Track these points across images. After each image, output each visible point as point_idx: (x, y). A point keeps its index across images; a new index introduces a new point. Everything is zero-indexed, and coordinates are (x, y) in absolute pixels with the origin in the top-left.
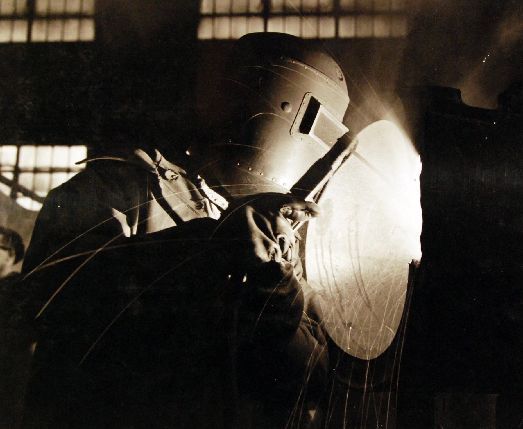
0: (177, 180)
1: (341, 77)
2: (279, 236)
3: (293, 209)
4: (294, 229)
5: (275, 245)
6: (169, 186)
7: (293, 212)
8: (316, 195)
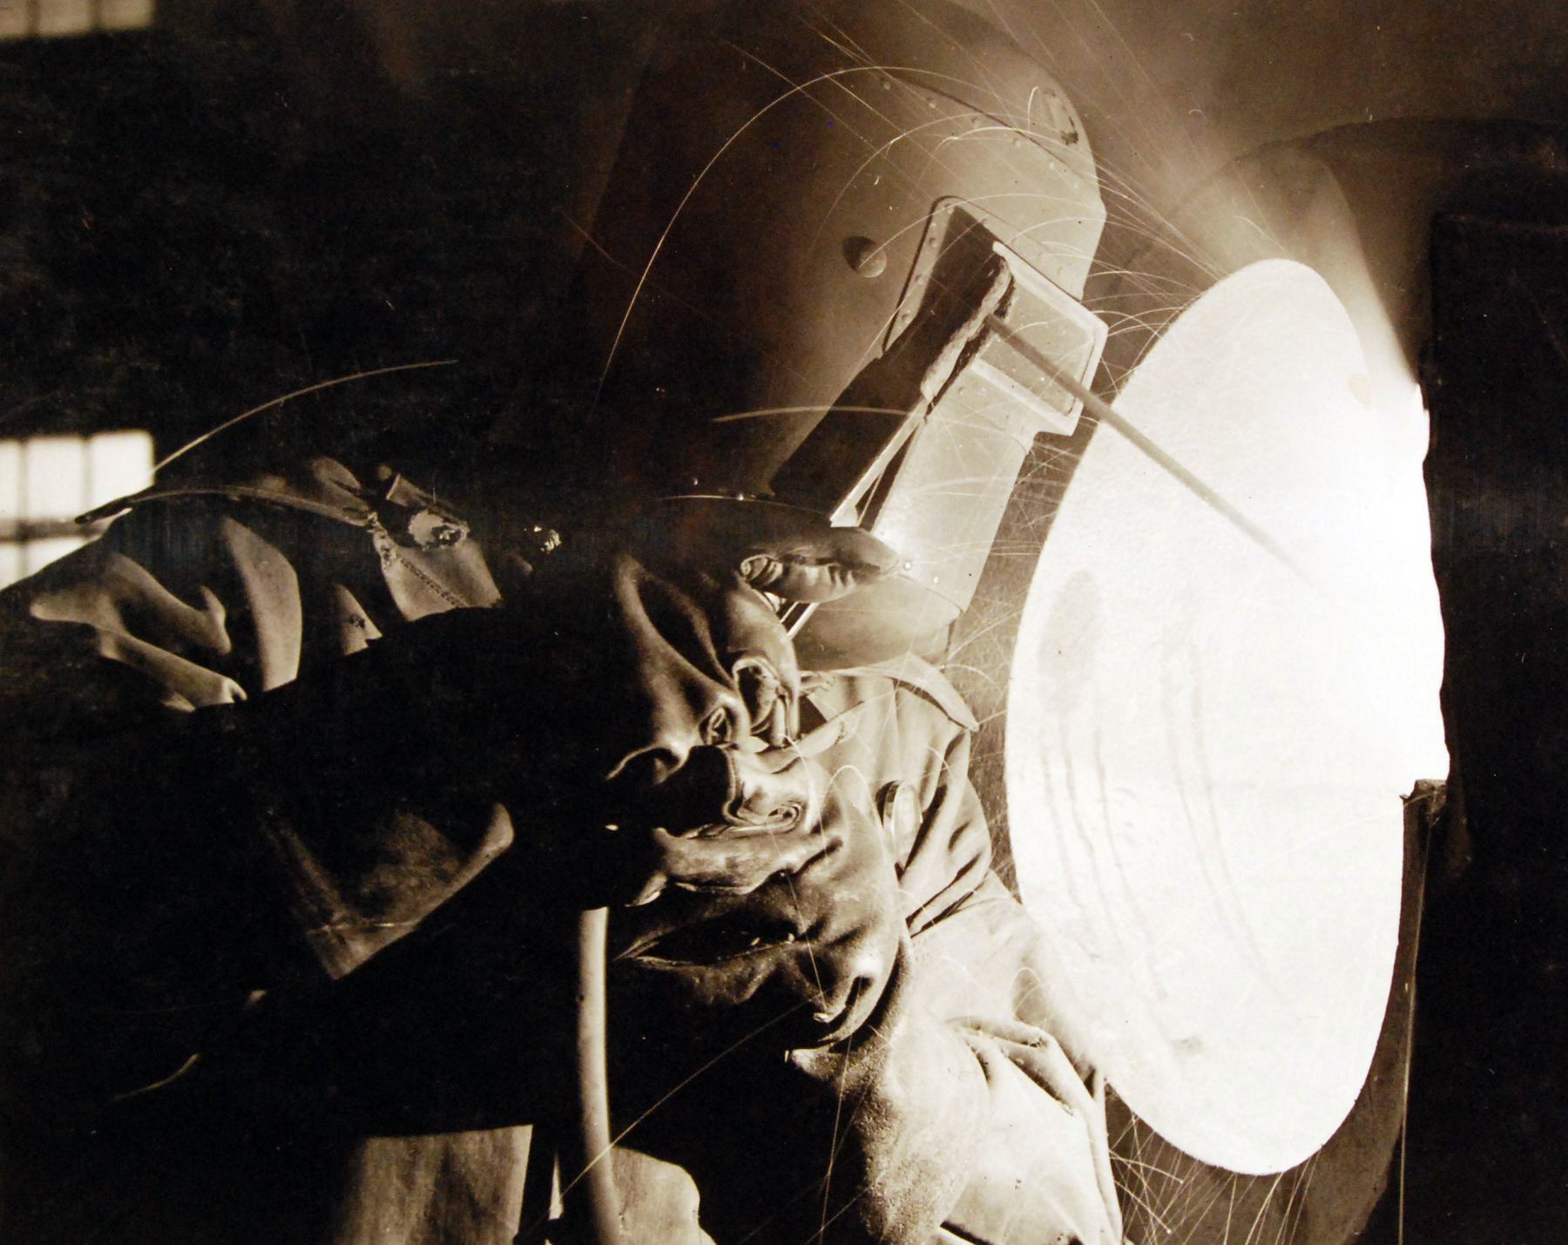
0: (457, 545)
1: (1069, 130)
2: (741, 664)
3: (787, 560)
4: (788, 624)
5: (728, 699)
6: (427, 572)
7: (786, 571)
8: (868, 493)
